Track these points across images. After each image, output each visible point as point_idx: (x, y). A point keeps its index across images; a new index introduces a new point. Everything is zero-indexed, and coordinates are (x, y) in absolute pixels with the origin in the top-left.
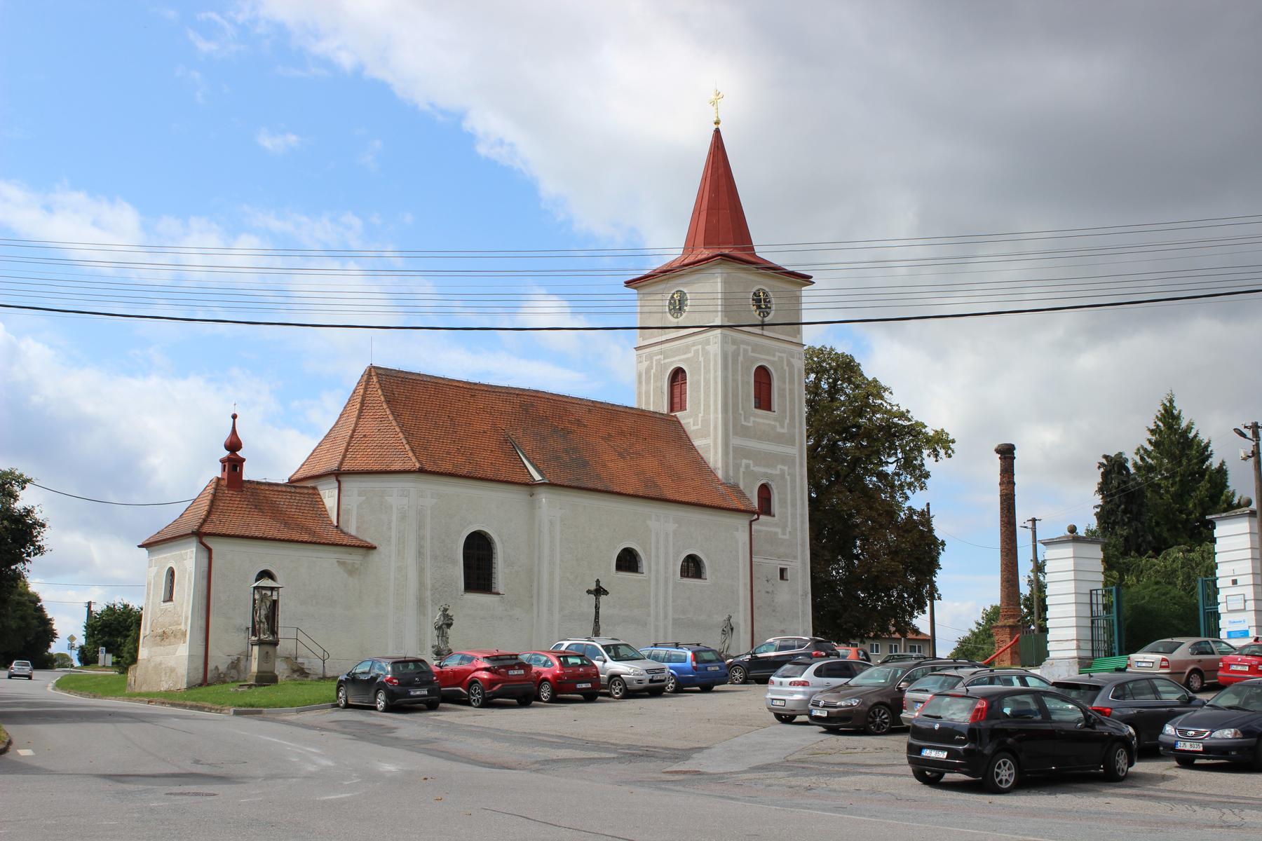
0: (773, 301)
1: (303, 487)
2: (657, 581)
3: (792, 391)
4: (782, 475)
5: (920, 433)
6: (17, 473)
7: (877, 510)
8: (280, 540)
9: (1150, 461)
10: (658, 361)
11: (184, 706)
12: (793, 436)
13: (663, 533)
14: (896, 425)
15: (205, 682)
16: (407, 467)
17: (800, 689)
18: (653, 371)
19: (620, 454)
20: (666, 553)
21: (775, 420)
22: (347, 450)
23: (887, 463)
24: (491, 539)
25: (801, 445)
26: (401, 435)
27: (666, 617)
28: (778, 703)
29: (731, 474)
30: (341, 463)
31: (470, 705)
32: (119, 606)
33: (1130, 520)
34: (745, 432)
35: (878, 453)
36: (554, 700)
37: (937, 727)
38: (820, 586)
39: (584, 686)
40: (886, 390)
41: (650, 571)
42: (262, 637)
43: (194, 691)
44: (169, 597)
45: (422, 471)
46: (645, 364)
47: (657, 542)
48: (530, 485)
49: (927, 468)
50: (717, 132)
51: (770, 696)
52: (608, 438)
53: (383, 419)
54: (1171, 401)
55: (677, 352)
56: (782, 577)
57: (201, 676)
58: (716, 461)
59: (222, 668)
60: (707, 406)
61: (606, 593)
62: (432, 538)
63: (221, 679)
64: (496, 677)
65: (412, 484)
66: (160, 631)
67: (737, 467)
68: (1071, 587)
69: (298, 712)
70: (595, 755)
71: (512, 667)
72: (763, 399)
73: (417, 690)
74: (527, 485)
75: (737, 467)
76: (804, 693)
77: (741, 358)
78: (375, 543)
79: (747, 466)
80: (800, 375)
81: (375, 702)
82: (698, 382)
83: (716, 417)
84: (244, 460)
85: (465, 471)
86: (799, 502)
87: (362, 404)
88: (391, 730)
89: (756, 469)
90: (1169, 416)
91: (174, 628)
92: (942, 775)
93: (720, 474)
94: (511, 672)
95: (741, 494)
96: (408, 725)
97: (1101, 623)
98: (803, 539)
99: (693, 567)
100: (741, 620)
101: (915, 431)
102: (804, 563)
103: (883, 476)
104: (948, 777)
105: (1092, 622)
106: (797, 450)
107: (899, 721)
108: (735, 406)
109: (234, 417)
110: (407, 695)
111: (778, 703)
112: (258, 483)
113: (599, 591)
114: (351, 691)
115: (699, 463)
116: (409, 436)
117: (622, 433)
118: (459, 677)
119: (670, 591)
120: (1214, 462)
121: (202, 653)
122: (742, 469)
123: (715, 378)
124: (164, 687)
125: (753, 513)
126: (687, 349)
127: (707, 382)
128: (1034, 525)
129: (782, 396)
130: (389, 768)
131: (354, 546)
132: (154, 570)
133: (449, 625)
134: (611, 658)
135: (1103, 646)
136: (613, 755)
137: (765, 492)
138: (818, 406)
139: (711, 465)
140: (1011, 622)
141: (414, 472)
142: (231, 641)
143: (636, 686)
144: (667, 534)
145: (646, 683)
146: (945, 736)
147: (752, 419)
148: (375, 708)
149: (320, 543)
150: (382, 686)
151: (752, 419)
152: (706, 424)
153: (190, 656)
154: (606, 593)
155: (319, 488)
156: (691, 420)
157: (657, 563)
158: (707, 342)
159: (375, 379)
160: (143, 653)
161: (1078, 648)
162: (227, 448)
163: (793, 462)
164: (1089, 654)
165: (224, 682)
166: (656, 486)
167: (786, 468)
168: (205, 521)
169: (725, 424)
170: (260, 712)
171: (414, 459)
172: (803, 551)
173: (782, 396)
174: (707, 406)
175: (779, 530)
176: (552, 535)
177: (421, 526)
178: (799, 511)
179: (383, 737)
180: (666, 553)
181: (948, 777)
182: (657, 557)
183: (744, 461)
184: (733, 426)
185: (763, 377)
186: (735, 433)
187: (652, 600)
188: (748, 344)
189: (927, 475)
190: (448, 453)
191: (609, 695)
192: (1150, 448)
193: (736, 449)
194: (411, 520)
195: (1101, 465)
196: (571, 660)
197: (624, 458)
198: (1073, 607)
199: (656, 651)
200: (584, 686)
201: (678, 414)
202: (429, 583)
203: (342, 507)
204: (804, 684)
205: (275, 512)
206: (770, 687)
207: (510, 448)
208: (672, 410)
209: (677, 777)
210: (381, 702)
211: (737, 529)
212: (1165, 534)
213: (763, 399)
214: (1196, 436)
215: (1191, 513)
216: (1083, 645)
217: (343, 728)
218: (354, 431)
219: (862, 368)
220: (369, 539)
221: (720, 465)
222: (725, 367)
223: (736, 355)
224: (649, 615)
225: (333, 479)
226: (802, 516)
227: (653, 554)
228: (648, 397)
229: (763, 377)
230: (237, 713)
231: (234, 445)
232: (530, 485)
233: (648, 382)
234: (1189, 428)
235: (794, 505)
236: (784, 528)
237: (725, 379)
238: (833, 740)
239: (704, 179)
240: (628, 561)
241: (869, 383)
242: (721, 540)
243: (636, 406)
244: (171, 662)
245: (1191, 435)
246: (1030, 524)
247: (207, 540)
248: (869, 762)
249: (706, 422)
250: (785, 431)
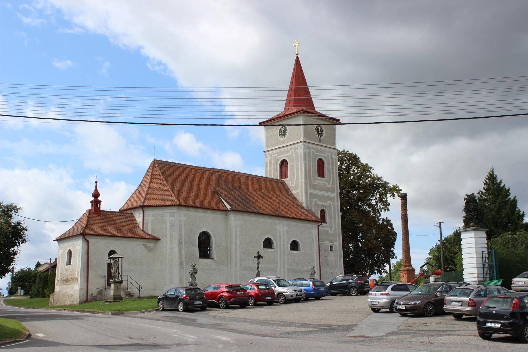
0: (324, 131)
1: (126, 213)
2: (280, 252)
3: (333, 169)
4: (330, 206)
5: (387, 186)
6: (14, 205)
7: (370, 220)
8: (118, 237)
9: (484, 197)
10: (275, 157)
11: (84, 312)
12: (334, 189)
13: (283, 231)
14: (376, 183)
15: (87, 301)
16: (174, 203)
17: (385, 297)
18: (272, 161)
19: (262, 197)
20: (284, 240)
21: (326, 182)
22: (146, 196)
23: (372, 200)
24: (210, 235)
25: (337, 192)
26: (170, 189)
27: (284, 268)
28: (375, 303)
29: (309, 205)
30: (144, 202)
31: (219, 308)
32: (26, 269)
33: (479, 222)
34: (314, 187)
35: (368, 196)
36: (256, 305)
37: (494, 312)
38: (346, 254)
39: (268, 298)
40: (371, 168)
41: (277, 247)
42: (115, 280)
43: (83, 305)
44: (69, 263)
45: (180, 205)
46: (269, 158)
47: (280, 235)
48: (226, 211)
49: (389, 202)
50: (297, 58)
51: (369, 300)
52: (256, 190)
53: (161, 183)
54: (492, 171)
55: (284, 152)
56: (331, 250)
57: (85, 298)
58: (302, 200)
59: (95, 294)
60: (297, 176)
61: (262, 257)
62: (185, 235)
63: (94, 299)
64: (232, 295)
65: (175, 211)
66: (65, 278)
67: (311, 202)
68: (474, 250)
69: (141, 313)
70: (311, 329)
71: (239, 290)
72: (321, 173)
73: (196, 302)
74: (225, 211)
75: (311, 202)
76: (387, 299)
77: (311, 155)
78: (160, 237)
79: (315, 202)
80: (336, 162)
81: (178, 307)
82: (293, 166)
83: (302, 180)
84: (101, 201)
85: (198, 205)
86: (337, 217)
87: (152, 176)
88: (195, 320)
89: (319, 203)
90: (492, 177)
91: (72, 277)
92: (491, 334)
93: (304, 205)
94: (238, 293)
95: (313, 214)
96: (200, 317)
97: (487, 266)
98: (339, 234)
99: (294, 246)
100: (317, 270)
101: (385, 186)
102: (340, 243)
103: (371, 205)
104: (495, 335)
105: (483, 265)
106: (336, 195)
107: (443, 310)
108: (310, 175)
109: (96, 182)
110: (193, 304)
111: (375, 303)
112: (107, 212)
113: (259, 257)
114: (165, 303)
115: (295, 201)
116: (173, 190)
117: (262, 188)
118: (213, 295)
119: (286, 257)
120: (511, 197)
121: (85, 287)
122: (313, 203)
123: (301, 164)
124: (68, 303)
125: (319, 222)
126: (288, 151)
127: (297, 165)
128: (440, 225)
129: (329, 171)
130: (224, 338)
131: (151, 239)
132: (61, 251)
133: (196, 273)
134: (278, 285)
135: (488, 276)
136: (315, 329)
137: (323, 212)
138: (343, 176)
139: (300, 201)
140: (407, 268)
141: (176, 206)
142: (98, 282)
143: (290, 298)
144: (284, 232)
145: (294, 297)
146: (497, 317)
147: (317, 181)
148: (178, 311)
149: (136, 238)
150: (181, 300)
151: (317, 181)
152: (297, 183)
153: (80, 289)
154: (262, 257)
155: (134, 213)
156: (290, 182)
157: (280, 244)
158: (297, 148)
159: (157, 165)
160: (57, 288)
161: (478, 277)
162: (93, 196)
163: (334, 199)
164: (482, 279)
165: (96, 300)
166: (279, 211)
167: (331, 202)
168: (85, 228)
169: (306, 184)
170: (123, 313)
171: (176, 200)
172: (339, 238)
173: (329, 171)
174: (297, 176)
175: (329, 229)
176: (235, 232)
177: (180, 230)
178: (337, 221)
179: (192, 323)
180: (284, 240)
181: (495, 335)
182: (280, 241)
183: (314, 200)
184: (309, 185)
185: (321, 163)
186: (310, 188)
187: (279, 261)
188: (314, 149)
189: (389, 205)
190: (190, 197)
191: (278, 302)
192: (484, 191)
193: (310, 194)
194: (175, 227)
195: (465, 199)
196: (261, 287)
197: (264, 199)
198: (475, 259)
199: (295, 282)
200: (268, 298)
201: (285, 180)
202: (184, 254)
203: (145, 222)
204: (387, 294)
205: (115, 224)
206: (370, 296)
207: (217, 194)
208: (281, 178)
209: (358, 339)
210: (181, 307)
211: (312, 229)
212: (493, 228)
213: (321, 173)
214: (504, 186)
215: (503, 219)
216: (480, 276)
217: (171, 319)
218: (149, 188)
219: (360, 160)
220: (157, 236)
221: (304, 201)
222: (305, 159)
223: (309, 153)
224: (277, 267)
225: (141, 210)
226: (338, 223)
227: (278, 240)
228: (270, 173)
229: (321, 163)
230: (112, 314)
231: (96, 195)
232: (226, 211)
233: (270, 166)
234: (500, 183)
235: (335, 218)
236: (331, 228)
237: (305, 164)
238: (405, 319)
239: (292, 78)
240: (268, 243)
241: (364, 165)
242: (307, 234)
243: (264, 176)
244: (71, 292)
245: (502, 186)
246: (438, 225)
247: (87, 237)
248: (440, 329)
249: (297, 183)
250: (330, 186)
